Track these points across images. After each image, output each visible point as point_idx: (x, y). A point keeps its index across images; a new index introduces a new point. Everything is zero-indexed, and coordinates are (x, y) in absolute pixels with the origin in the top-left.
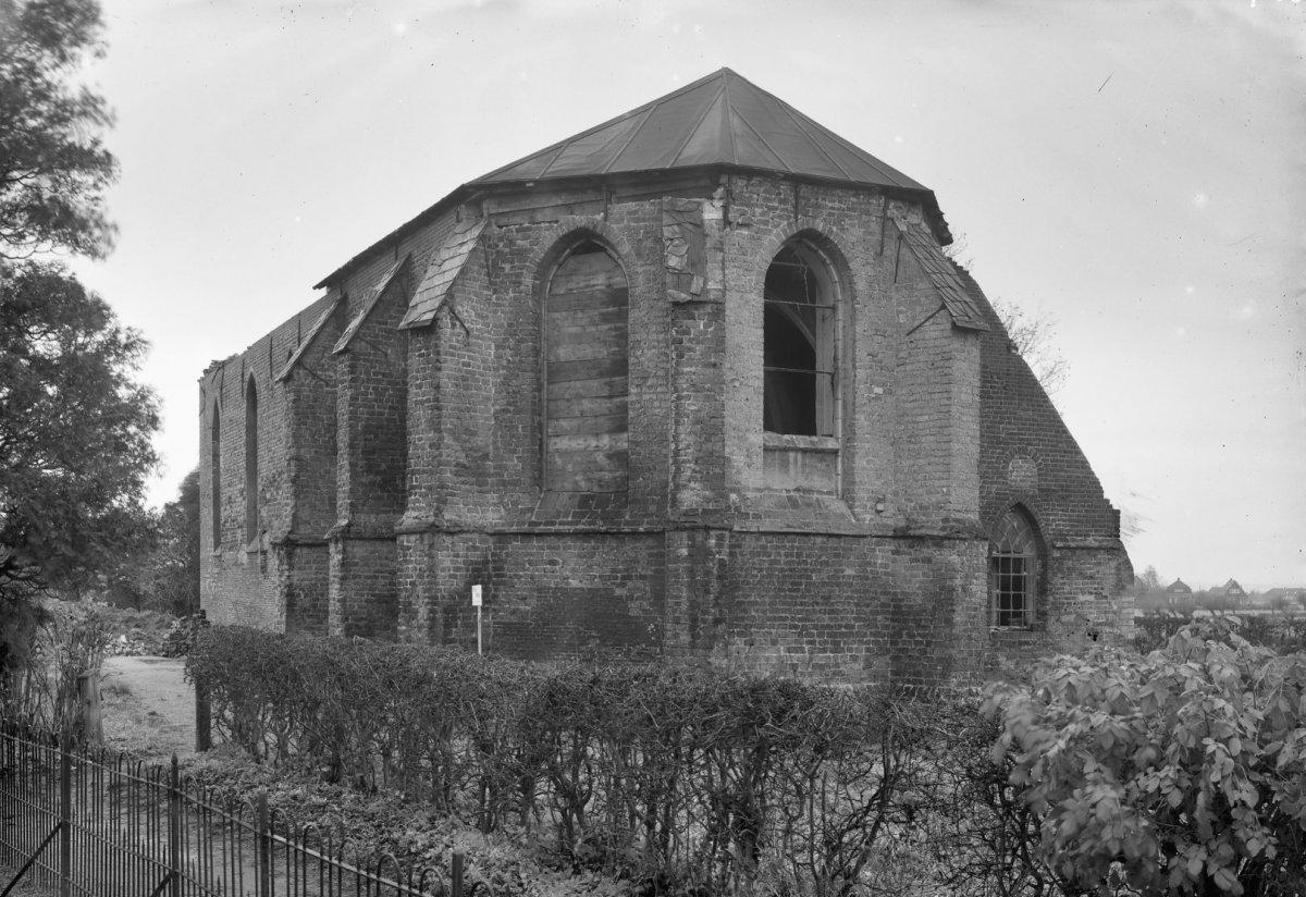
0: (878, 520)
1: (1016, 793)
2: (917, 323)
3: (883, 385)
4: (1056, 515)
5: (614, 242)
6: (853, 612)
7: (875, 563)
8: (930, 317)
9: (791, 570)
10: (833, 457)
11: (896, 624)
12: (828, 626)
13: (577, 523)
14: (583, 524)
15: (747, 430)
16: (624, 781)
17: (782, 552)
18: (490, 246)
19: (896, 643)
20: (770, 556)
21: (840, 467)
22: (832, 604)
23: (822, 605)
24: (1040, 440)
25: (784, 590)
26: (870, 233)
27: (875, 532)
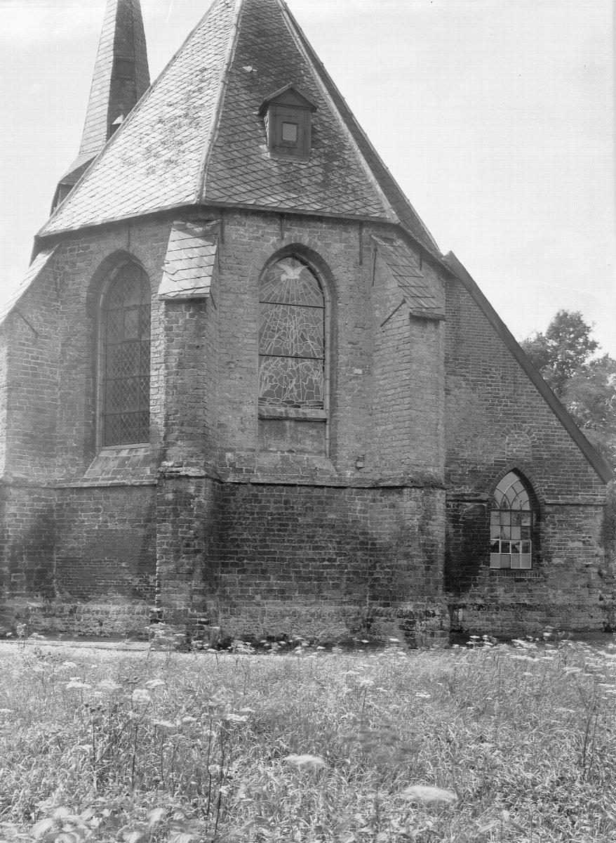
0: (357, 475)
2: (387, 317)
3: (362, 367)
4: (548, 478)
5: (141, 259)
6: (334, 548)
8: (396, 310)
9: (279, 514)
11: (372, 558)
16: (328, 753)
17: (272, 500)
18: (58, 268)
19: (371, 574)
20: (260, 502)
21: (328, 433)
22: (316, 542)
23: (307, 542)
25: (273, 530)
26: (351, 247)
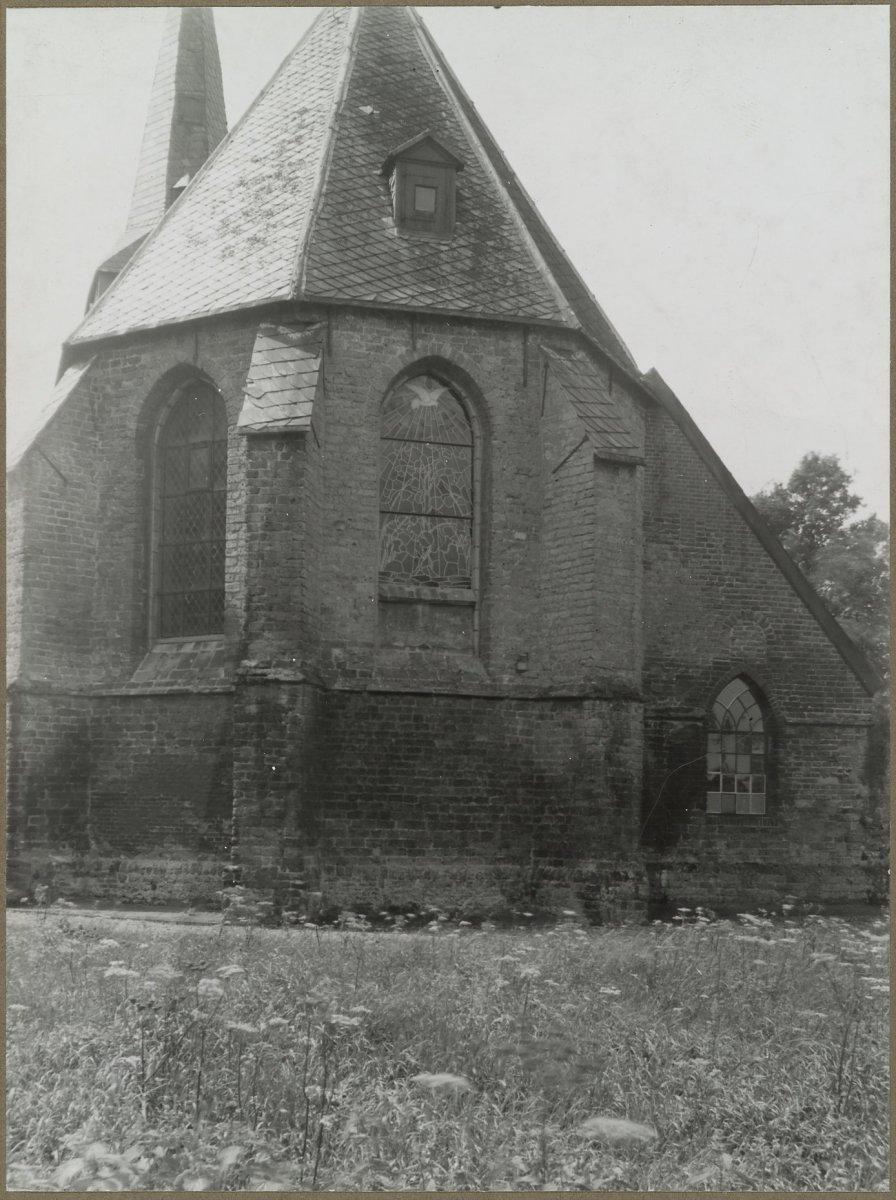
0: (519, 681)
1: (478, 1068)
7: (514, 730)
8: (575, 451)
10: (470, 611)
12: (452, 799)
13: (172, 684)
14: (179, 685)
15: (354, 578)
21: (476, 621)
24: (768, 604)
26: (511, 361)
27: (512, 694)
